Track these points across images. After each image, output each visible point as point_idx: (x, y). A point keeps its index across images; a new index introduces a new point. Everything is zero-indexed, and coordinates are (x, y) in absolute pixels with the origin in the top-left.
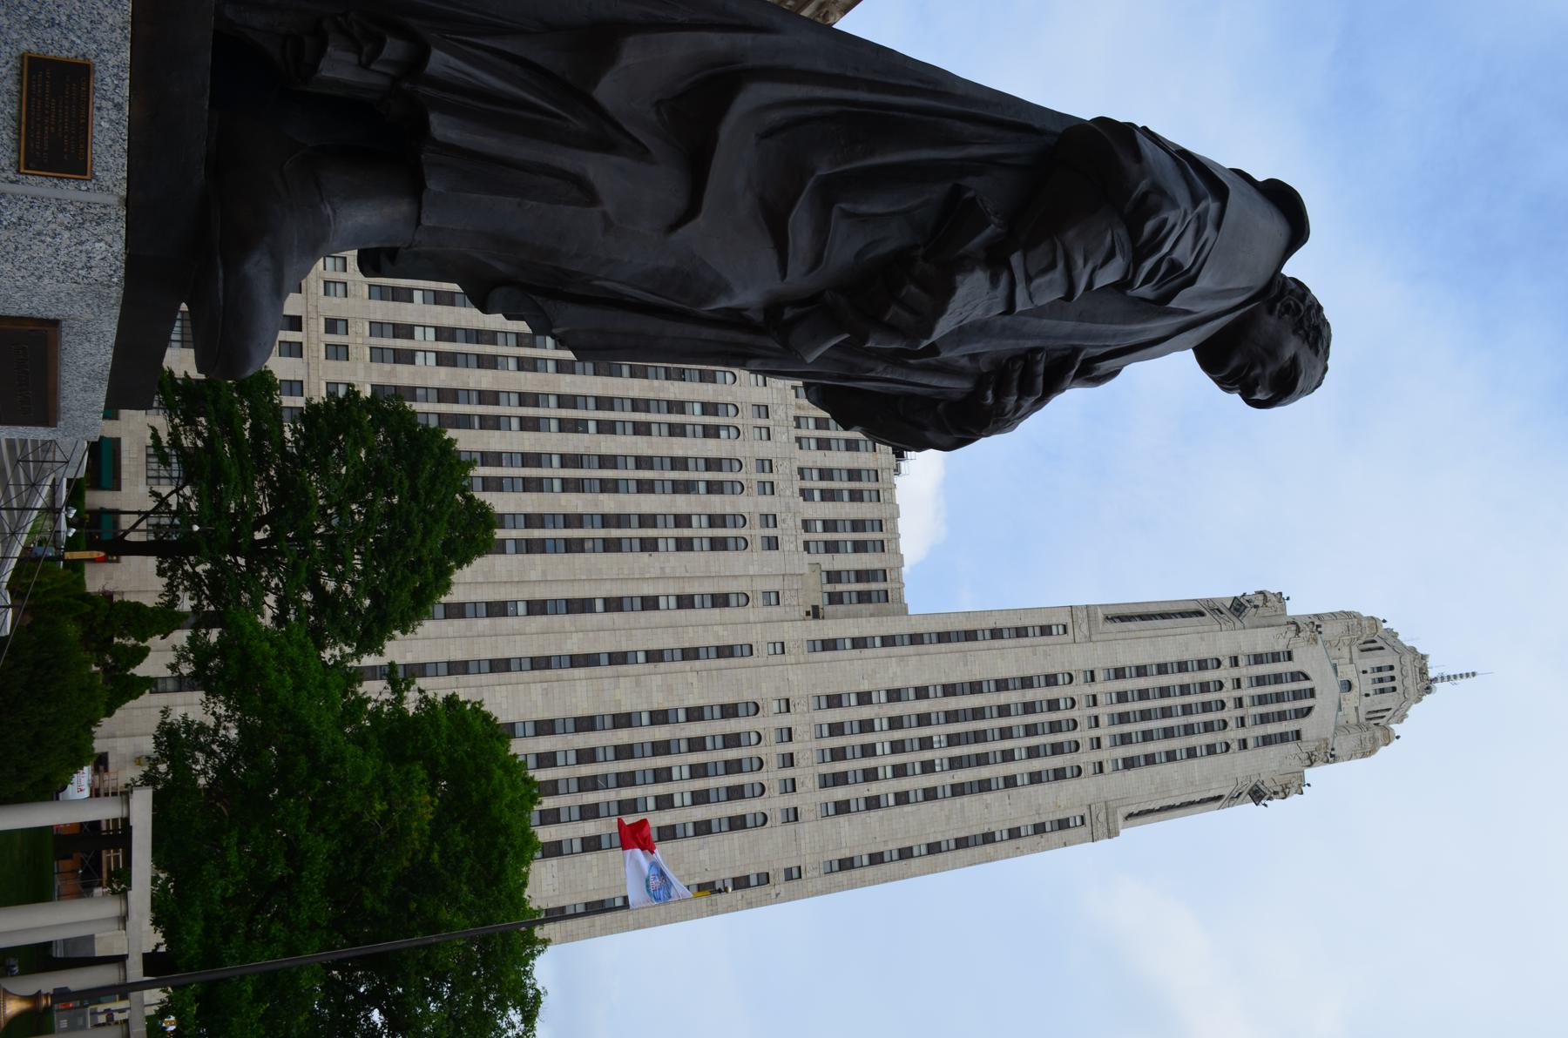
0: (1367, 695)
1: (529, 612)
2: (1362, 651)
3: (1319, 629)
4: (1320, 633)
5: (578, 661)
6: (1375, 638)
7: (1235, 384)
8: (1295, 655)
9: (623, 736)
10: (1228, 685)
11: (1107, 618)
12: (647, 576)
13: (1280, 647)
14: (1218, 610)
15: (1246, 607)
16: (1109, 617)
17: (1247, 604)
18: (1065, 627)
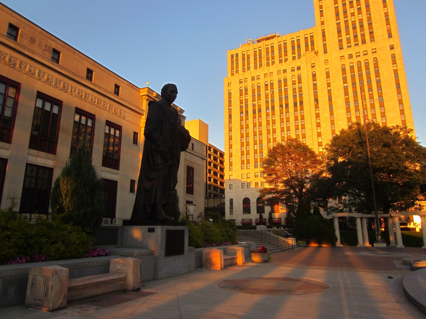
7: (66, 267)
12: (309, 98)
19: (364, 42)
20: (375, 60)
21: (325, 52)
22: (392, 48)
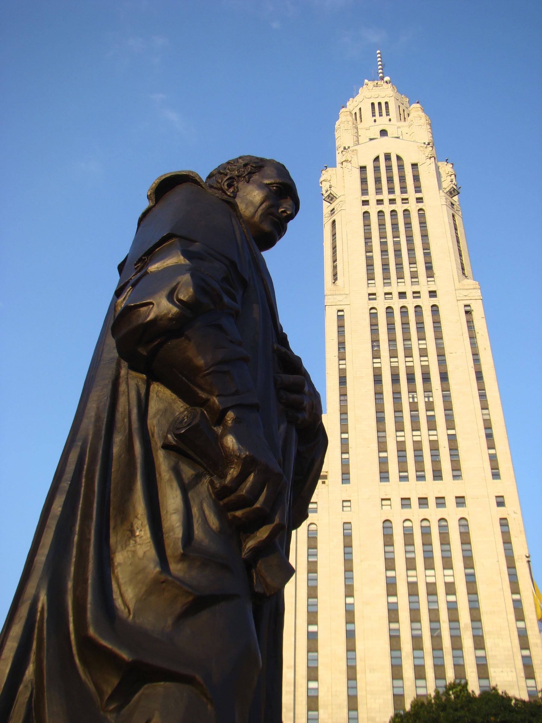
0: (390, 120)
1: (316, 679)
2: (361, 121)
3: (347, 148)
4: (349, 147)
5: (351, 648)
6: (353, 113)
8: (363, 164)
9: (404, 615)
10: (380, 208)
11: (334, 283)
13: (357, 173)
14: (331, 211)
15: (331, 193)
16: (333, 281)
17: (329, 192)
18: (339, 311)
19: (438, 475)
20: (463, 522)
21: (346, 478)
22: (500, 503)
